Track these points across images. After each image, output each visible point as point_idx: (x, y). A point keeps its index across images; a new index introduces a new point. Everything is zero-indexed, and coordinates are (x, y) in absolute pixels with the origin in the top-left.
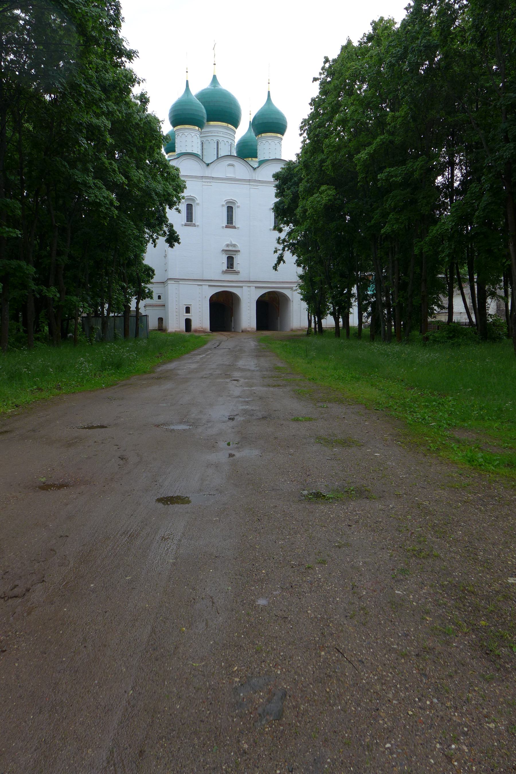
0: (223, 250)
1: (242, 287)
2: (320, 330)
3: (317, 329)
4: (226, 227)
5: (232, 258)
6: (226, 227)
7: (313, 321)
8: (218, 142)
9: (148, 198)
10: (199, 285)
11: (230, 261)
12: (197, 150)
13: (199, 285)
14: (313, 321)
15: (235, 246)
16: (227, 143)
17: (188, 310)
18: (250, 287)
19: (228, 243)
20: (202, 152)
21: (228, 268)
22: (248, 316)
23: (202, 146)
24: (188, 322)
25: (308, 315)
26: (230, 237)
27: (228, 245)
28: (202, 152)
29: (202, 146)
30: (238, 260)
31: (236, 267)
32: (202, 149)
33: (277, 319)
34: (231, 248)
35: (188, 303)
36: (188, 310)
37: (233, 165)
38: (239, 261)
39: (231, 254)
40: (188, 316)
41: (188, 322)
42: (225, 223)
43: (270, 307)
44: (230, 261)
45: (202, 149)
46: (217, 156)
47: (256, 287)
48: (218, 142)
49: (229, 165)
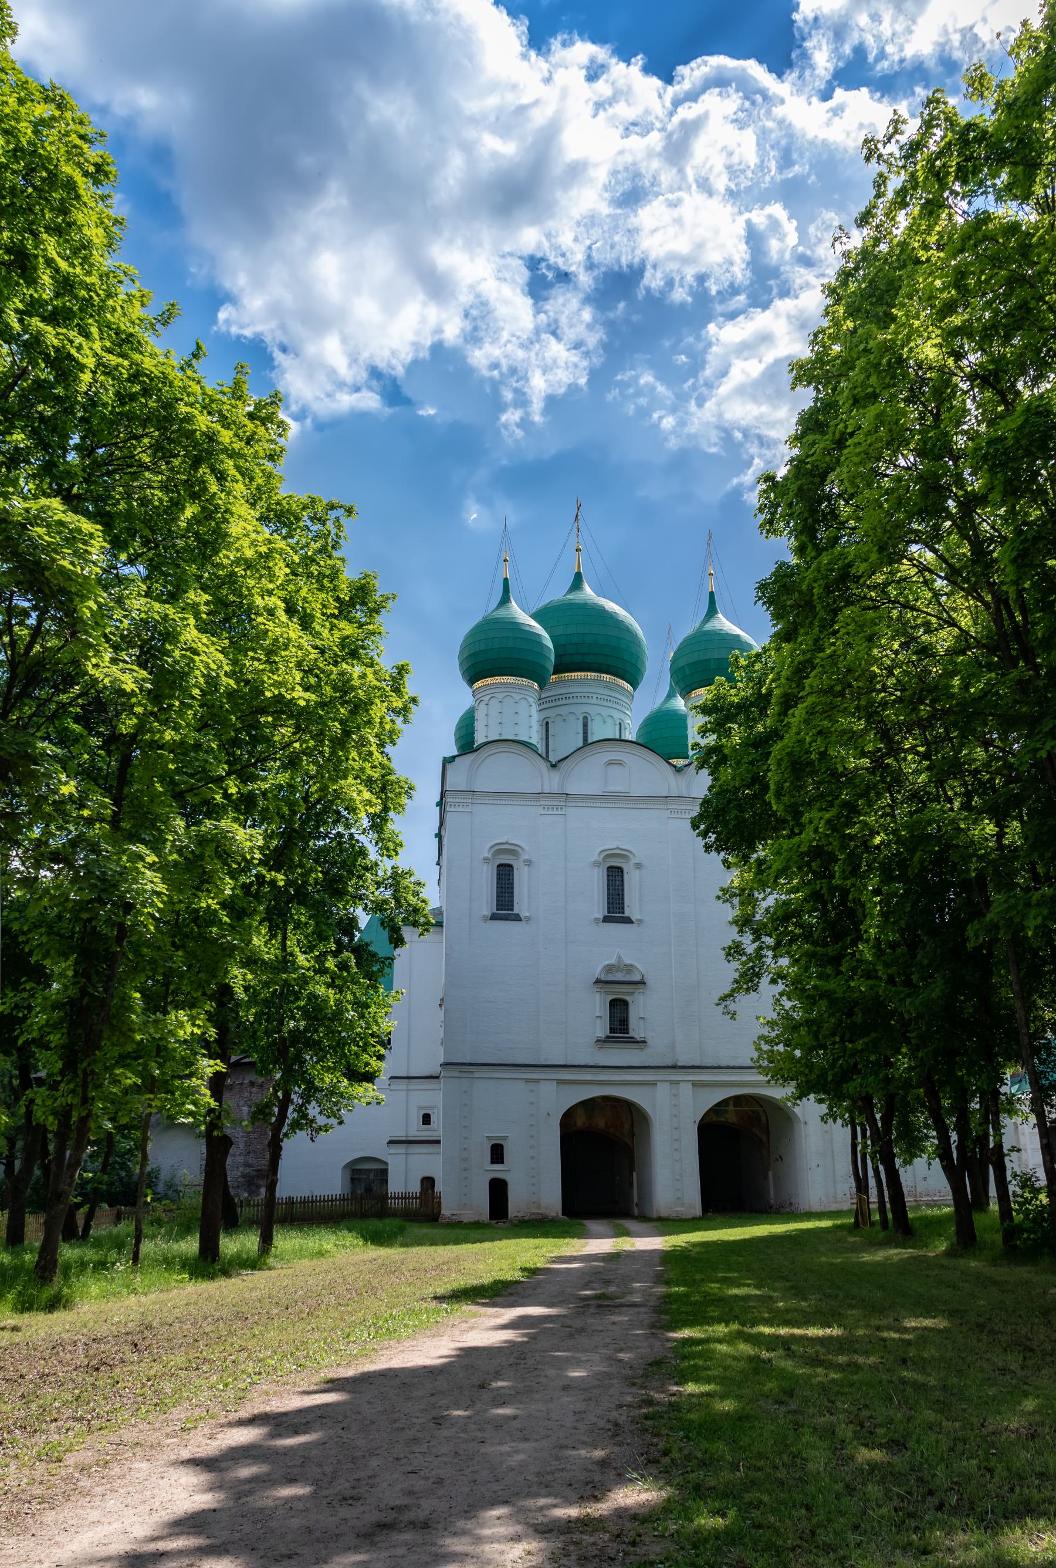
0: (598, 981)
1: (653, 1084)
2: (900, 1224)
3: (890, 1216)
4: (606, 920)
5: (624, 1004)
6: (606, 920)
7: (872, 1182)
8: (585, 718)
9: (703, 368)
10: (527, 1080)
11: (619, 1016)
12: (535, 737)
13: (527, 1080)
14: (872, 1182)
15: (629, 968)
16: (609, 721)
17: (497, 1153)
18: (677, 1082)
19: (612, 961)
20: (547, 745)
21: (612, 1030)
22: (673, 1168)
23: (547, 731)
24: (498, 1189)
25: (854, 1146)
26: (615, 947)
27: (609, 969)
28: (547, 745)
29: (547, 731)
30: (640, 1008)
31: (636, 1029)
32: (547, 738)
33: (766, 1177)
34: (619, 977)
35: (497, 1132)
36: (497, 1153)
37: (620, 763)
38: (644, 1012)
39: (619, 993)
40: (498, 1171)
41: (498, 1189)
42: (599, 909)
43: (740, 1155)
44: (619, 1016)
45: (547, 738)
46: (585, 739)
47: (695, 1084)
48: (585, 718)
49: (610, 763)
